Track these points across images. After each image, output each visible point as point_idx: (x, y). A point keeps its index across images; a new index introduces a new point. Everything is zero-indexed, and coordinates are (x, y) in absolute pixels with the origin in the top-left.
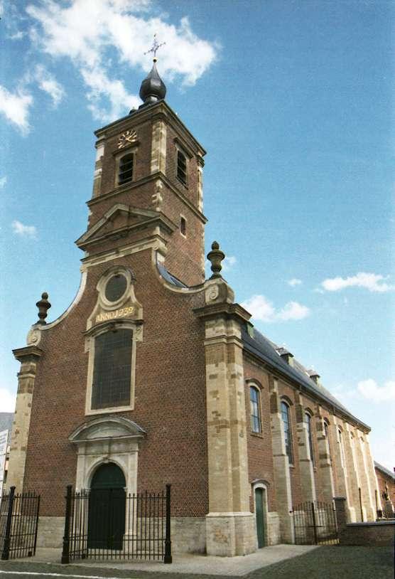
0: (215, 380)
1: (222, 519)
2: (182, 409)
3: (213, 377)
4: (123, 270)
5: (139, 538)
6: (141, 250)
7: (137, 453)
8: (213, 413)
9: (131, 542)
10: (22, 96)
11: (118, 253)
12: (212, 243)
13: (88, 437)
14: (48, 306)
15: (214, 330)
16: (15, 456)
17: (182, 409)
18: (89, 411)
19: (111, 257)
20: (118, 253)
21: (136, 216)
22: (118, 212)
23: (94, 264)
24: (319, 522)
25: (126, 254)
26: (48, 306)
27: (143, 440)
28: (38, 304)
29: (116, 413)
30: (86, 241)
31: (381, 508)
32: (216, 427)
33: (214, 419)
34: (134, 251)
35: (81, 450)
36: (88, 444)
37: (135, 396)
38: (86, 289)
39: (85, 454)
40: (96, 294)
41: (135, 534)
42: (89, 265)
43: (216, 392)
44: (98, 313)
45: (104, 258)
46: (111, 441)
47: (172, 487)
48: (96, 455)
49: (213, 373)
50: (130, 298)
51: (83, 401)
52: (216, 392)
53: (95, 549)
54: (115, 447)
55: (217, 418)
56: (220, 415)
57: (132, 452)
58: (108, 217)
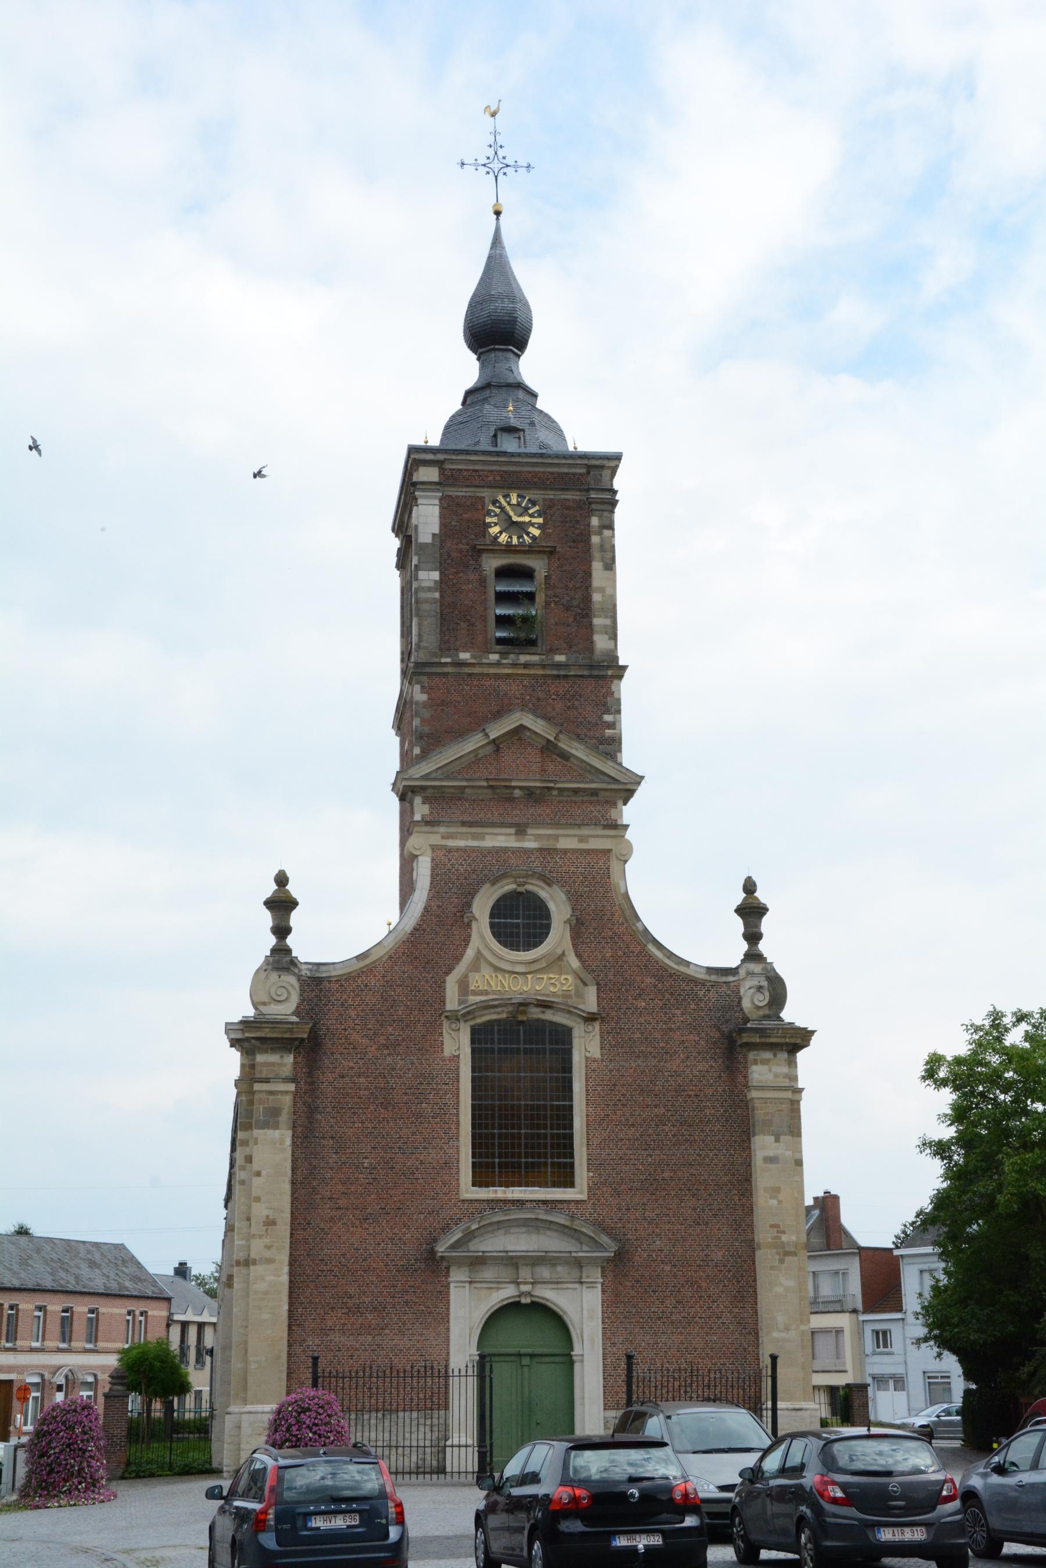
0: (773, 1166)
1: (793, 1413)
2: (695, 1209)
3: (770, 1160)
4: (543, 885)
5: (394, 1451)
7: (599, 1286)
8: (772, 1226)
9: (394, 1451)
12: (742, 882)
13: (472, 1248)
14: (292, 904)
15: (770, 1070)
16: (270, 1278)
17: (695, 1209)
18: (469, 1191)
19: (500, 839)
20: (521, 831)
21: (565, 756)
23: (451, 843)
24: (470, 1387)
25: (546, 844)
26: (292, 904)
28: (270, 904)
30: (425, 777)
32: (778, 1253)
33: (774, 1238)
34: (564, 844)
35: (457, 1275)
36: (478, 1262)
37: (589, 1170)
38: (430, 899)
39: (470, 1282)
40: (462, 919)
41: (380, 1437)
43: (777, 1190)
44: (475, 967)
45: (481, 837)
46: (536, 1261)
47: (779, 1360)
48: (498, 1284)
49: (771, 1154)
50: (563, 954)
51: (450, 1165)
52: (777, 1190)
54: (545, 1272)
55: (779, 1238)
56: (784, 1232)
57: (591, 1285)
58: (492, 736)
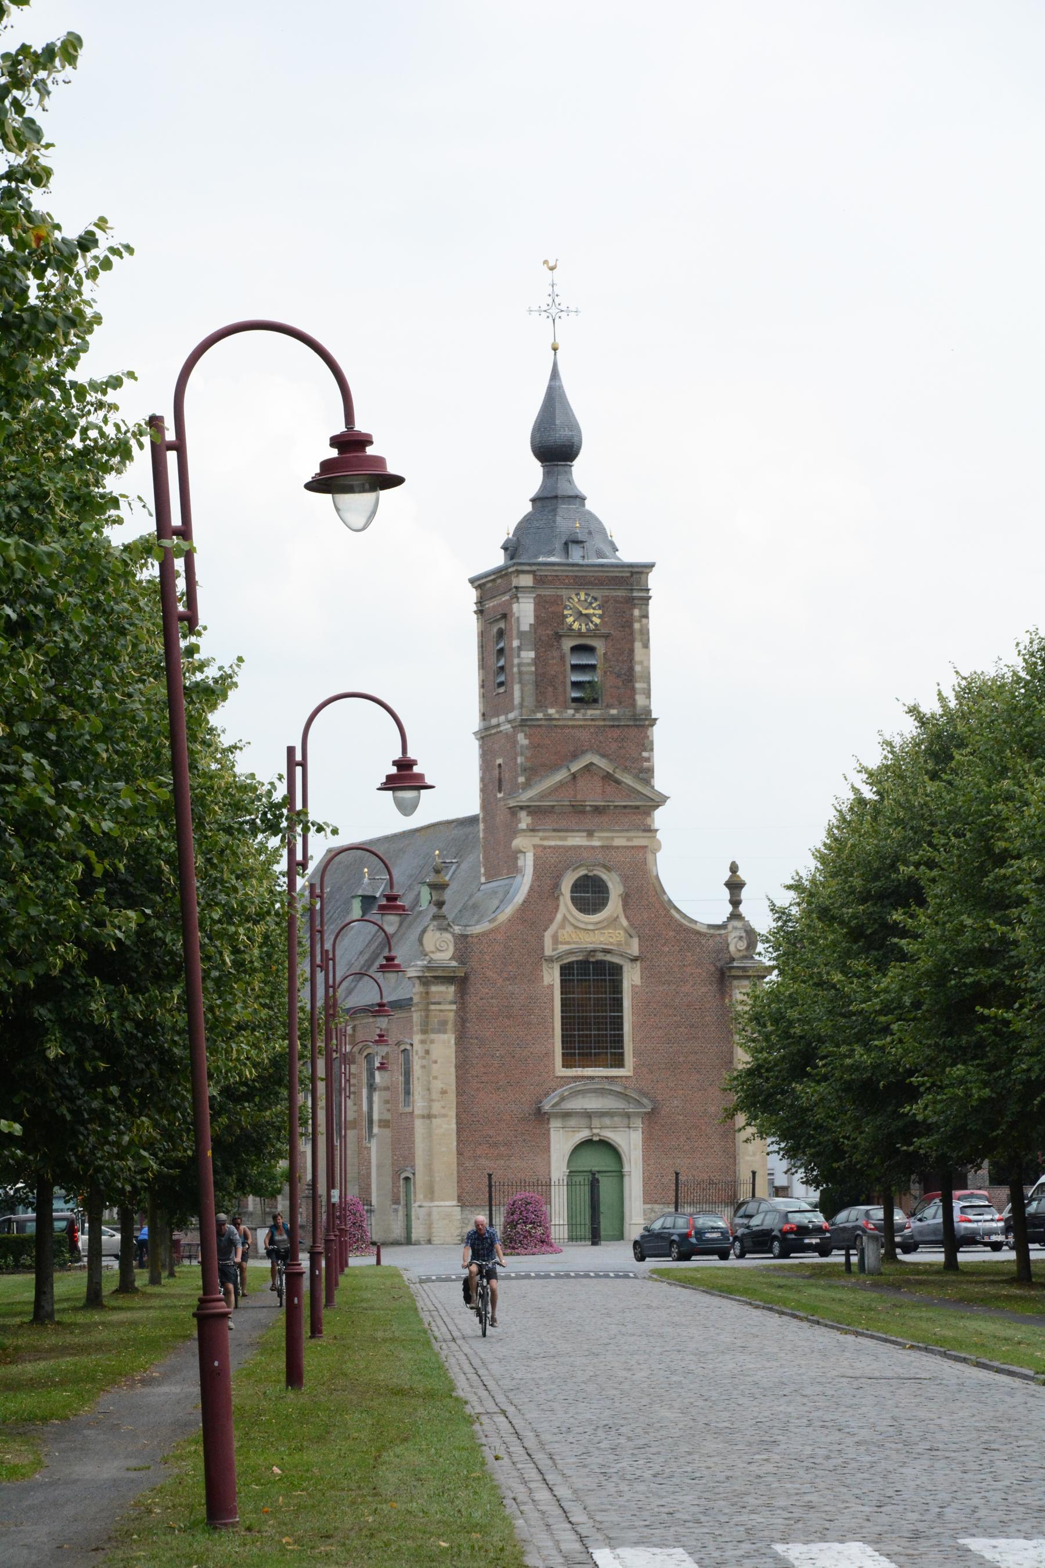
6: (630, 844)
10: (818, 1191)
11: (590, 834)
16: (445, 1126)
20: (590, 834)
22: (589, 768)
23: (546, 843)
27: (651, 1117)
29: (606, 1077)
31: (677, 1515)
34: (617, 842)
36: (567, 1115)
42: (537, 841)
44: (562, 926)
45: (565, 839)
48: (577, 1129)
51: (549, 1054)
53: (52, 1211)
57: (636, 1129)
